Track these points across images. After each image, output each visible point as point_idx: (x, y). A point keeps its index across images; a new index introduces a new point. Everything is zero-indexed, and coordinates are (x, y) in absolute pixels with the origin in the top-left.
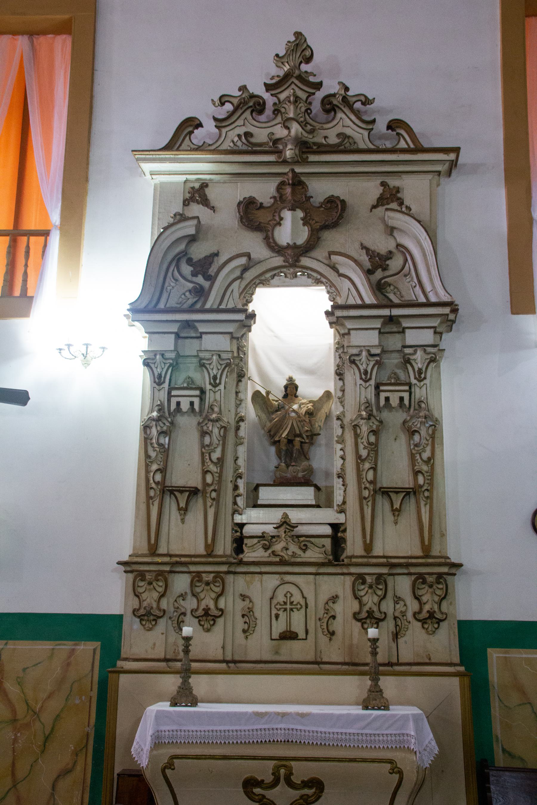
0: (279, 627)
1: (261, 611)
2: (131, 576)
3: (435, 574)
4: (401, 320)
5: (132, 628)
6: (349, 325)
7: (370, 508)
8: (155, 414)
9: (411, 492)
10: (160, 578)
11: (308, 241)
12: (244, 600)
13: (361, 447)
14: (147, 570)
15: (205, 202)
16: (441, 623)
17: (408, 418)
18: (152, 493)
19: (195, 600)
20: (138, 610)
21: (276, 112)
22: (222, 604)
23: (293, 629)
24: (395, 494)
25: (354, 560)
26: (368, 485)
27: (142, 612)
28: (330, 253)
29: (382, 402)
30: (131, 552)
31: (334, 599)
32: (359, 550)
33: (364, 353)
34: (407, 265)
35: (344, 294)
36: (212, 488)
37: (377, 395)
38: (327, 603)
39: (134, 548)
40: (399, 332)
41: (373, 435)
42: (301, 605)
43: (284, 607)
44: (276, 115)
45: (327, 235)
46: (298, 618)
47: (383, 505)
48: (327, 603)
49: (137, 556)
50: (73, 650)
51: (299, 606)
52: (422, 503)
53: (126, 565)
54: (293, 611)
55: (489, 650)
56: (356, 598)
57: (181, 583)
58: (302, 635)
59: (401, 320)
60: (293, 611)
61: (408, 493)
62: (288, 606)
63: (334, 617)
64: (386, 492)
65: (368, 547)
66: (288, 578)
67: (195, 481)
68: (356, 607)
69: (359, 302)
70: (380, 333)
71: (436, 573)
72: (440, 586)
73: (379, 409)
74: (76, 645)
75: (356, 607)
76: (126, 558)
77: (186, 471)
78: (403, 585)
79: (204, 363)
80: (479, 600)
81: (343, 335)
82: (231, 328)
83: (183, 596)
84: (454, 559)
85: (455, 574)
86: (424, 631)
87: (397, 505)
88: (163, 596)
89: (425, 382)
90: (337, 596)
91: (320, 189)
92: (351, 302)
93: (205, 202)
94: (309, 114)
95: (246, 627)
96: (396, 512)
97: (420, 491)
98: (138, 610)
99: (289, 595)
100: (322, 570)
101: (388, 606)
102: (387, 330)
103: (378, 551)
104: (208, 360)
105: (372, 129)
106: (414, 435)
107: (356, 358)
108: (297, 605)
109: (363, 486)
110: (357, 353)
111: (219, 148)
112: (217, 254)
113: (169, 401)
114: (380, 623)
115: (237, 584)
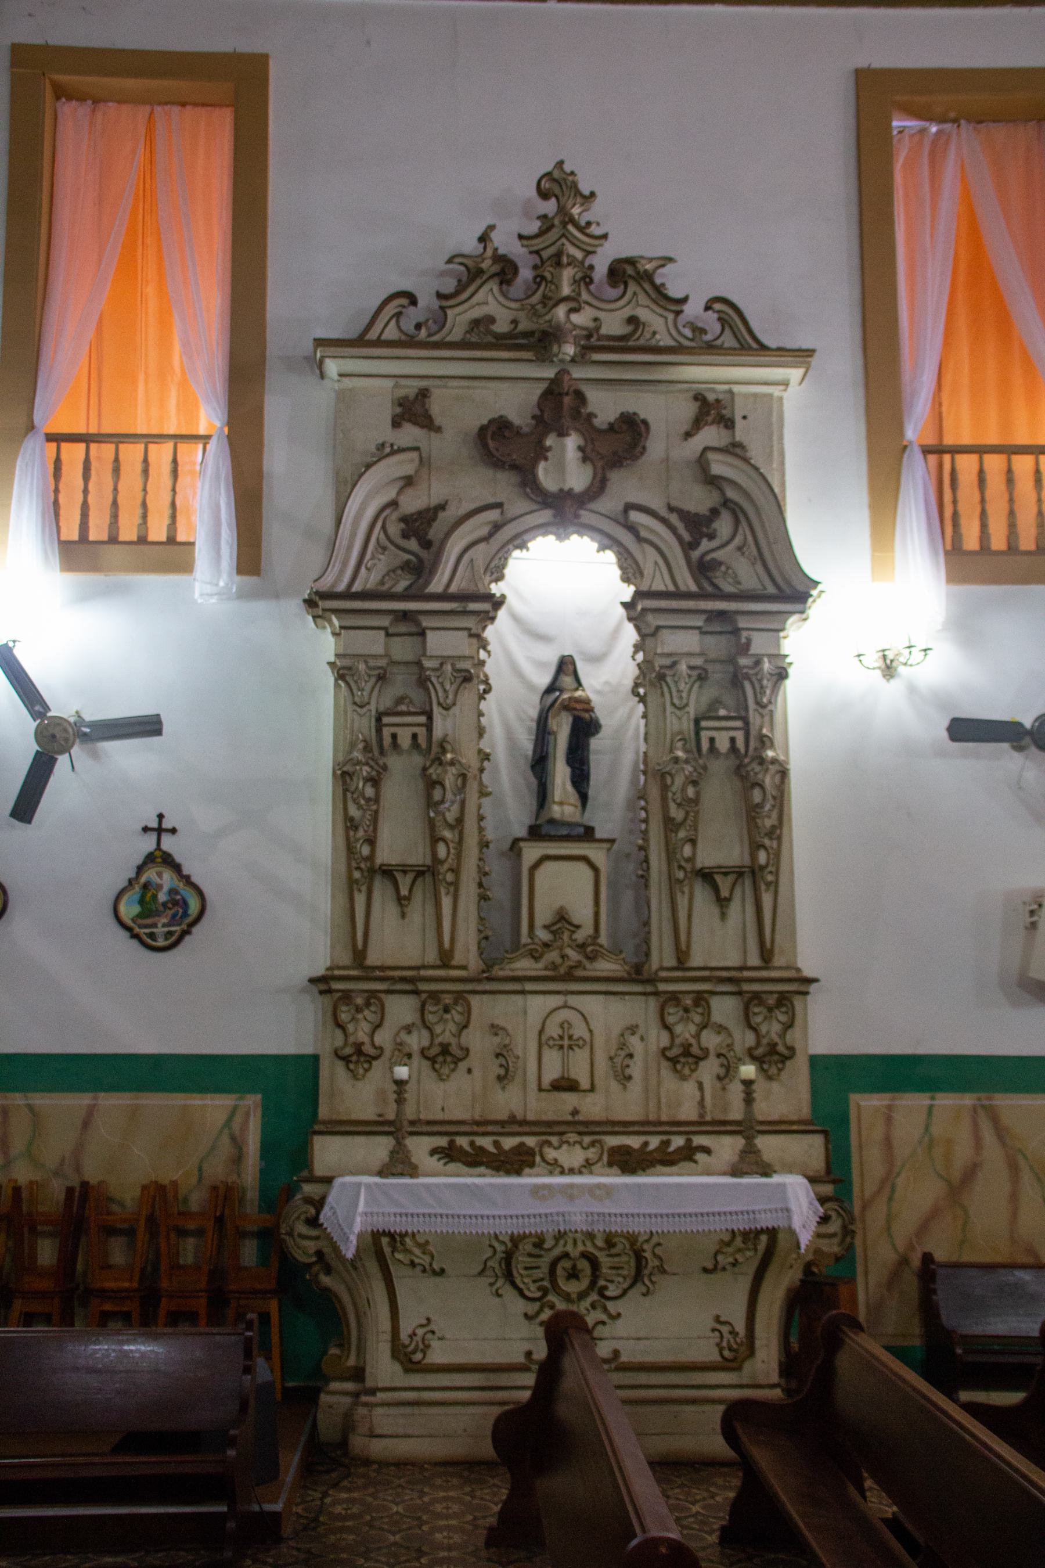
0: (552, 1073)
1: (526, 1047)
2: (327, 999)
3: (776, 992)
4: (421, 618)
5: (333, 1076)
6: (653, 620)
7: (687, 896)
8: (357, 755)
9: (426, 872)
10: (372, 1001)
11: (587, 491)
12: (496, 1034)
13: (673, 806)
14: (346, 987)
15: (427, 423)
16: (374, 1063)
17: (428, 764)
18: (450, 877)
19: (425, 1033)
20: (429, 1049)
21: (538, 280)
22: (464, 1040)
23: (573, 1076)
24: (401, 874)
25: (423, 973)
26: (683, 864)
27: (675, 1052)
28: (629, 507)
29: (387, 740)
30: (328, 964)
31: (633, 1029)
32: (670, 961)
33: (448, 668)
34: (740, 531)
35: (648, 569)
36: (446, 866)
37: (379, 731)
38: (622, 1035)
39: (332, 960)
40: (731, 633)
41: (373, 786)
42: (584, 1040)
43: (561, 1043)
44: (539, 285)
45: (615, 477)
46: (581, 1056)
47: (381, 889)
48: (622, 1035)
49: (339, 968)
50: (94, 1106)
51: (551, 1043)
52: (443, 891)
53: (322, 983)
54: (572, 1049)
55: (855, 1098)
56: (751, 1027)
57: (401, 1010)
58: (585, 1084)
59: (421, 618)
60: (572, 1049)
61: (741, 874)
62: (566, 1042)
63: (631, 1056)
64: (388, 872)
65: (682, 956)
66: (572, 1000)
67: (419, 857)
68: (665, 1040)
69: (671, 588)
70: (388, 635)
71: (774, 992)
72: (700, 1010)
73: (382, 752)
74: (240, 1098)
75: (665, 1040)
76: (320, 971)
77: (398, 840)
78: (725, 1009)
79: (746, 673)
80: (827, 1029)
81: (647, 637)
82: (385, 621)
83: (408, 1029)
84: (808, 973)
85: (807, 993)
86: (433, 1075)
87: (404, 892)
88: (378, 1026)
89: (687, 709)
90: (637, 1026)
91: (605, 406)
92: (659, 586)
93: (427, 423)
94: (587, 285)
95: (502, 1072)
96: (402, 901)
97: (757, 874)
98: (429, 1049)
99: (566, 1025)
100: (479, 987)
101: (711, 1040)
102: (709, 629)
103: (697, 959)
104: (752, 668)
105: (681, 311)
106: (434, 788)
107: (668, 672)
108: (578, 1040)
109: (354, 864)
110: (437, 666)
111: (448, 339)
112: (442, 507)
113: (697, 734)
114: (374, 1063)
115: (485, 1009)
